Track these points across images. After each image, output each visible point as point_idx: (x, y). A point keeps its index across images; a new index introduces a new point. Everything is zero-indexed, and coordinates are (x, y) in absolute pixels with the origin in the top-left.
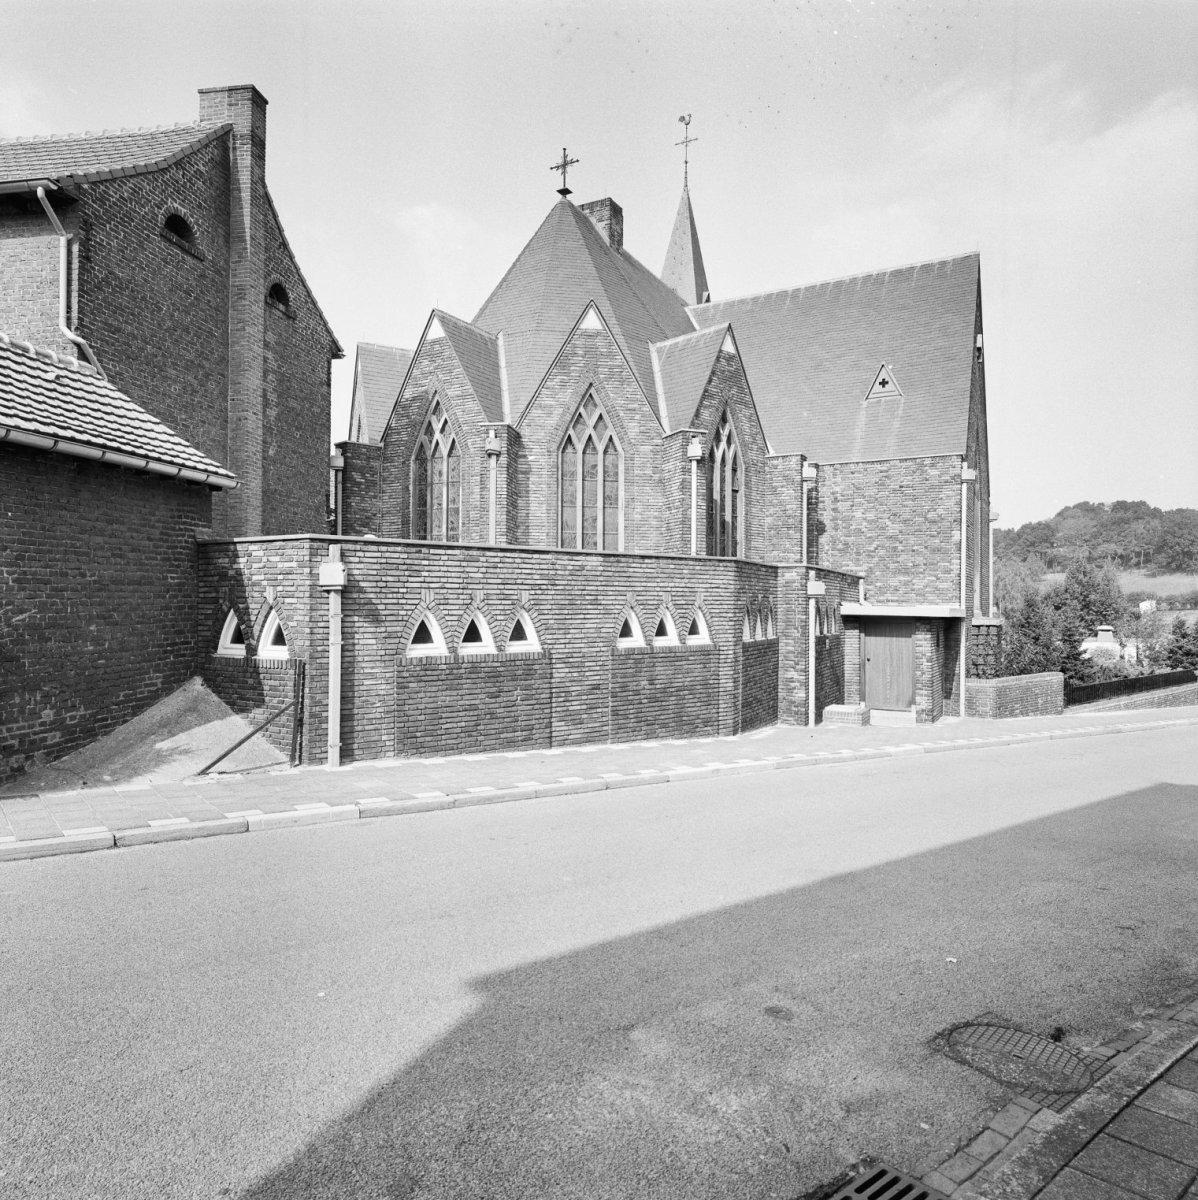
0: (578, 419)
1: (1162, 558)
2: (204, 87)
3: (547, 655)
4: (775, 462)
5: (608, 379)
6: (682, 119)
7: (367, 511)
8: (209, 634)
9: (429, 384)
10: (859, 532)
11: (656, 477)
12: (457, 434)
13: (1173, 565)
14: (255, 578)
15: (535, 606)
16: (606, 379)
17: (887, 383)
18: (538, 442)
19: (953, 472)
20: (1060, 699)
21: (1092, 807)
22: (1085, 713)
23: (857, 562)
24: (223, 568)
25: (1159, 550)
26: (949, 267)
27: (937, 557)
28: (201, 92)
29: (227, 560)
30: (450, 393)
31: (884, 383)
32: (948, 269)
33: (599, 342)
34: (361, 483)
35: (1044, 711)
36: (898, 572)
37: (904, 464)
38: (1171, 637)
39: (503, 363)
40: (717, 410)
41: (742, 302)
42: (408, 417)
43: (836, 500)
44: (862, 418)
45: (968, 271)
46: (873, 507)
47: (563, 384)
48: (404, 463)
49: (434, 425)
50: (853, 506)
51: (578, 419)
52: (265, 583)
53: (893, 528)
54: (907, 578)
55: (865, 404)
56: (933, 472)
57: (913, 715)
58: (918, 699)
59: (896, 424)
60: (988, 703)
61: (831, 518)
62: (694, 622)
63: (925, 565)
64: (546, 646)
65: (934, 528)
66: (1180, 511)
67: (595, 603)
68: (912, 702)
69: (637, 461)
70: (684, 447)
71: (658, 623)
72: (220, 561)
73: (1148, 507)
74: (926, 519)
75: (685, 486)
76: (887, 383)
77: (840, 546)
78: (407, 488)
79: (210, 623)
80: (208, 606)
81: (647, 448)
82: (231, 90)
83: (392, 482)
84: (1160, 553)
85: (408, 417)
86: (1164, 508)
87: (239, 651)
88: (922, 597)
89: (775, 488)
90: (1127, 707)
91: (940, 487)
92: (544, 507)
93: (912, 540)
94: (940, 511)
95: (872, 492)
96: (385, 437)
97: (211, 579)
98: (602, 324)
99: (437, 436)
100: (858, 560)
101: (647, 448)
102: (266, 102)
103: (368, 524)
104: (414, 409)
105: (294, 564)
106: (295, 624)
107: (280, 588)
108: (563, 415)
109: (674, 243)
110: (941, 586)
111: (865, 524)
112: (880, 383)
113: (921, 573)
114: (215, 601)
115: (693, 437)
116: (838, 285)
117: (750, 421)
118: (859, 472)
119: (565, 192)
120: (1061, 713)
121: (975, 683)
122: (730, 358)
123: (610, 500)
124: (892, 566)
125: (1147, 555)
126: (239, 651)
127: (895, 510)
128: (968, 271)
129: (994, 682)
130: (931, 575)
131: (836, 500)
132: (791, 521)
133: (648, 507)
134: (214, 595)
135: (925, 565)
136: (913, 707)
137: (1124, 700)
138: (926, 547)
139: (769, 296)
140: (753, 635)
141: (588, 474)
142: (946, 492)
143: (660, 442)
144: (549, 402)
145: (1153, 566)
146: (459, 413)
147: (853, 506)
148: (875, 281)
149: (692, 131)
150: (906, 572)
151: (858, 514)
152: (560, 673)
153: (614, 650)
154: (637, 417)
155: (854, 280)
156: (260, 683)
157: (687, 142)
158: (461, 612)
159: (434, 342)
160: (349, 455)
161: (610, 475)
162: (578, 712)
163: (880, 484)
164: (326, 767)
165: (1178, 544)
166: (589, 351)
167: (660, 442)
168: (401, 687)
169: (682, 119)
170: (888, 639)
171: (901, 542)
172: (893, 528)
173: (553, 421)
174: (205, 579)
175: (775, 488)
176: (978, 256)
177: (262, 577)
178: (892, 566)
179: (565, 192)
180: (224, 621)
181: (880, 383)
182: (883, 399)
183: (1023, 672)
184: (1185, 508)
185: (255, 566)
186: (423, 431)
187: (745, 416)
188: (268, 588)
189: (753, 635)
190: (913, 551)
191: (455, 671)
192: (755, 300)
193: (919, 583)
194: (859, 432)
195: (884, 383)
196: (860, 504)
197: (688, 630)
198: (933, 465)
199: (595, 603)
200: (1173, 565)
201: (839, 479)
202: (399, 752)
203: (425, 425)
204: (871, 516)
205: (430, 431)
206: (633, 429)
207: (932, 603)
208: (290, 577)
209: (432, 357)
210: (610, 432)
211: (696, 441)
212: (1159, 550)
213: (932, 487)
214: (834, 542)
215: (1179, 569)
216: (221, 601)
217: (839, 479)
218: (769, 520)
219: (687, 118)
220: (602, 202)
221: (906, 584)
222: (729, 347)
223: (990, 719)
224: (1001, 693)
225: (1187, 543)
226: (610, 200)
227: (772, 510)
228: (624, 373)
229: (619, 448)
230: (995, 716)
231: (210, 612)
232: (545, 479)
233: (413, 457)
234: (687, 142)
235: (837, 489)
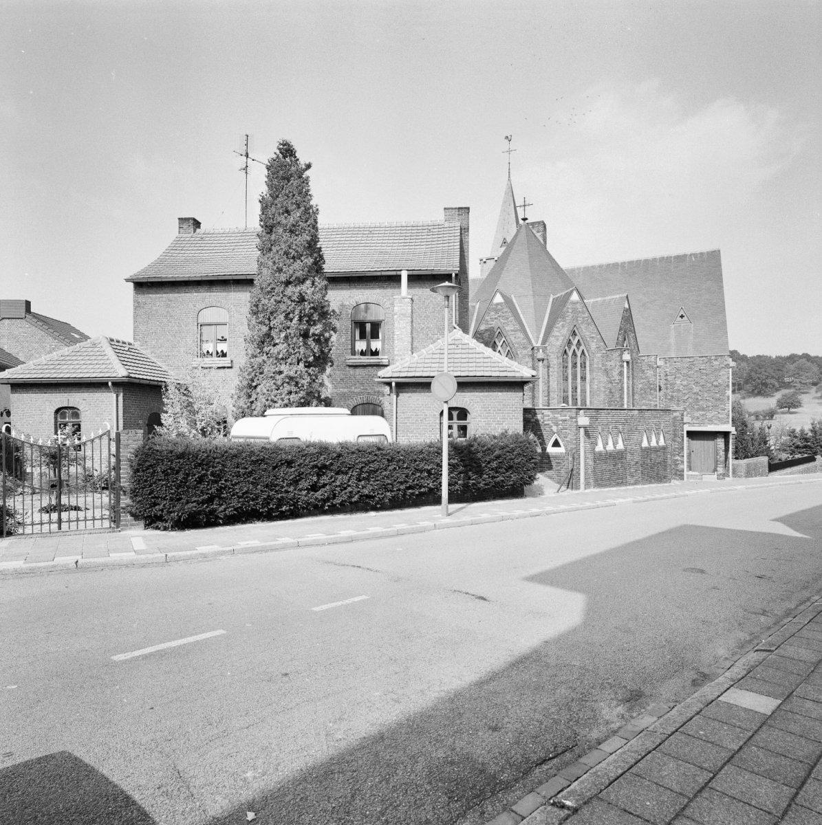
0: (570, 343)
1: (748, 387)
2: (447, 207)
4: (643, 358)
5: (582, 323)
6: (507, 137)
9: (494, 324)
10: (679, 391)
11: (603, 368)
13: (756, 391)
14: (546, 422)
16: (582, 323)
18: (553, 353)
19: (725, 363)
20: (767, 470)
21: (758, 534)
22: (777, 475)
23: (678, 405)
25: (747, 382)
26: (705, 256)
27: (718, 403)
28: (445, 209)
30: (507, 328)
31: (682, 316)
32: (705, 256)
35: (762, 475)
36: (699, 410)
37: (702, 359)
39: (520, 312)
41: (593, 267)
43: (667, 375)
44: (673, 333)
45: (715, 256)
47: (563, 326)
49: (498, 343)
51: (570, 343)
53: (696, 389)
54: (703, 413)
55: (673, 326)
57: (716, 476)
58: (718, 469)
59: (691, 338)
60: (742, 471)
65: (717, 389)
66: (759, 357)
68: (715, 470)
70: (621, 355)
73: (739, 354)
75: (621, 373)
77: (669, 397)
81: (599, 355)
82: (459, 208)
84: (747, 384)
86: (749, 355)
88: (711, 421)
89: (644, 371)
90: (791, 473)
93: (706, 395)
94: (720, 381)
101: (599, 355)
104: (487, 335)
109: (503, 211)
110: (720, 416)
111: (682, 387)
116: (646, 261)
118: (678, 362)
120: (767, 476)
121: (737, 462)
123: (583, 379)
124: (696, 407)
125: (739, 385)
128: (715, 256)
129: (746, 461)
131: (667, 375)
132: (652, 386)
133: (600, 382)
136: (716, 473)
137: (789, 470)
139: (608, 265)
140: (649, 442)
141: (575, 365)
142: (722, 372)
143: (605, 352)
144: (558, 334)
145: (743, 392)
148: (666, 260)
149: (513, 145)
150: (703, 409)
151: (678, 382)
152: (629, 457)
155: (655, 260)
156: (550, 461)
157: (509, 151)
159: (498, 304)
161: (583, 366)
163: (690, 368)
164: (581, 491)
165: (759, 379)
166: (574, 310)
167: (605, 352)
169: (507, 137)
170: (702, 442)
172: (696, 389)
173: (559, 343)
175: (644, 371)
176: (719, 251)
178: (696, 407)
182: (682, 325)
183: (752, 456)
184: (761, 355)
189: (615, 444)
192: (601, 266)
193: (709, 415)
194: (672, 340)
196: (679, 378)
200: (756, 391)
201: (668, 365)
202: (595, 487)
204: (685, 383)
206: (593, 346)
207: (716, 424)
209: (497, 311)
210: (582, 347)
211: (626, 352)
212: (747, 382)
213: (716, 370)
215: (760, 394)
217: (668, 365)
218: (640, 386)
219: (509, 137)
220: (539, 223)
221: (703, 415)
223: (744, 478)
224: (748, 465)
225: (764, 377)
226: (543, 222)
227: (642, 381)
229: (587, 355)
230: (746, 477)
232: (556, 370)
234: (509, 151)
235: (668, 370)
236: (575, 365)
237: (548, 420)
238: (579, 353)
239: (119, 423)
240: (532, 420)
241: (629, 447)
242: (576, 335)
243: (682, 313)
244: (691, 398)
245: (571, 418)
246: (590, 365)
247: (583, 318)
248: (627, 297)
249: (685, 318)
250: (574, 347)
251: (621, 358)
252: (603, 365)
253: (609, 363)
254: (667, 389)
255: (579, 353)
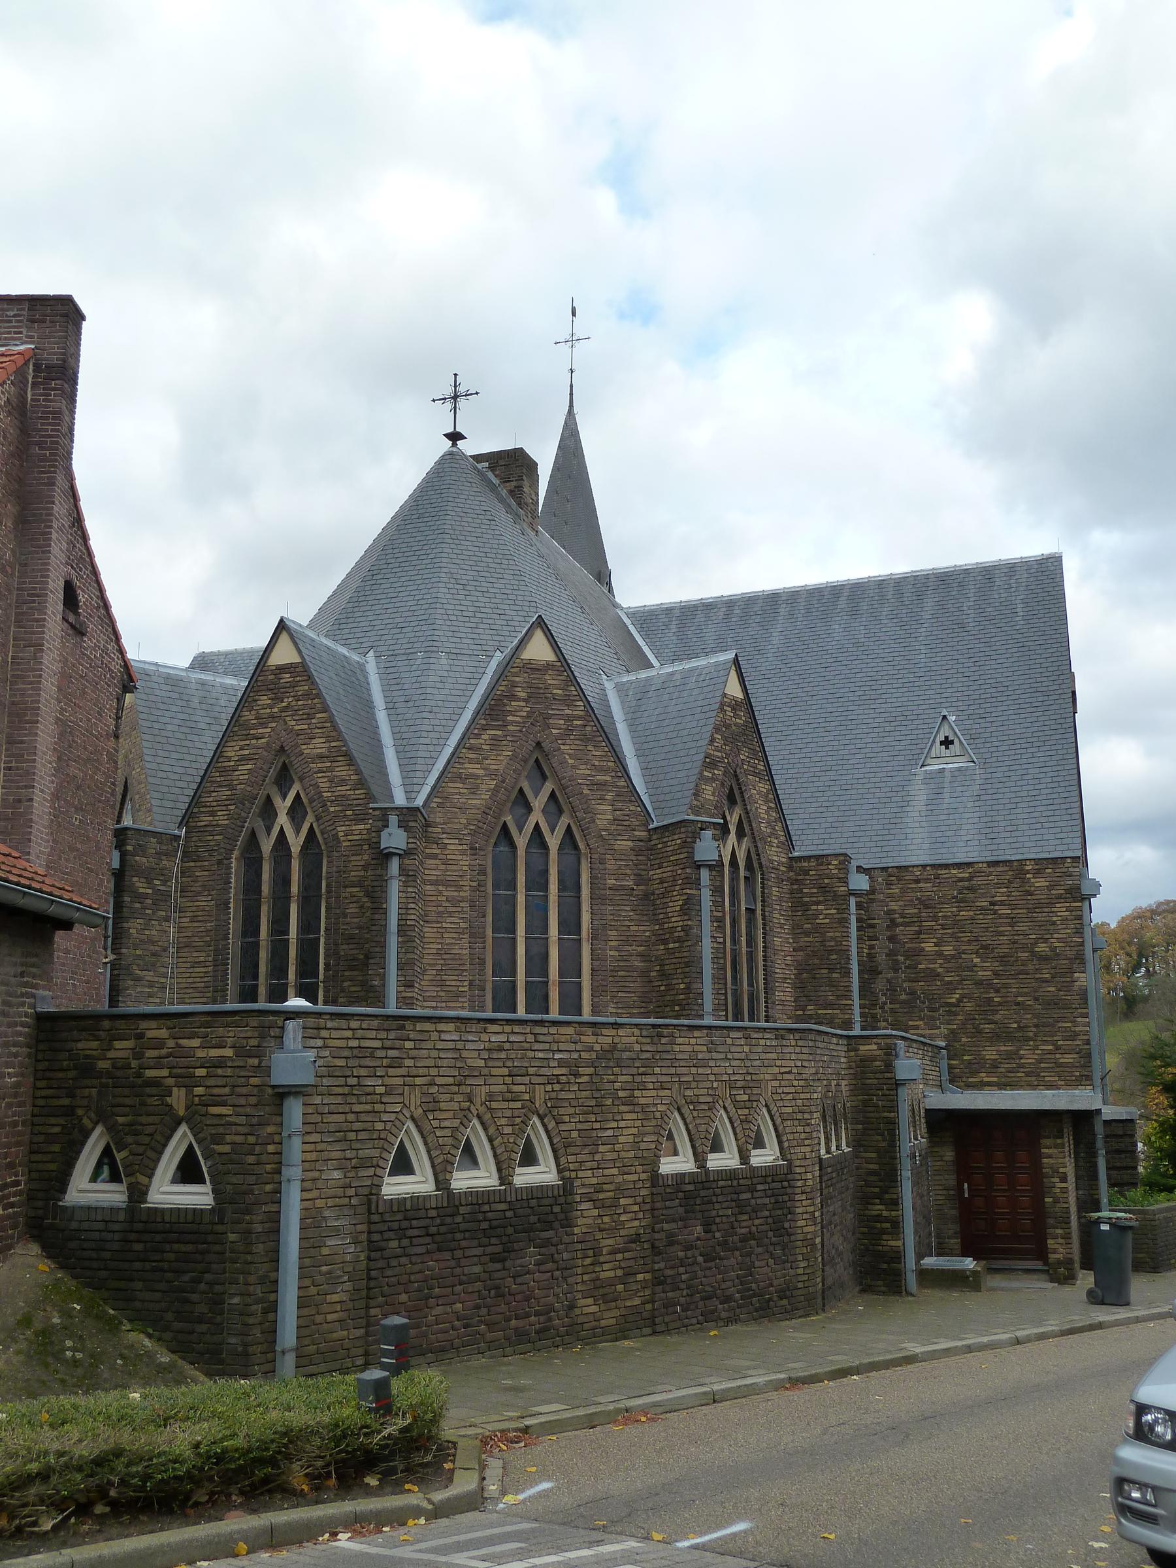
3: (567, 1186)
5: (564, 736)
7: (153, 943)
8: (53, 1167)
10: (932, 975)
12: (318, 818)
14: (150, 1073)
15: (550, 1114)
16: (564, 736)
17: (952, 742)
24: (87, 1057)
29: (95, 1044)
30: (307, 750)
31: (947, 743)
33: (551, 679)
34: (146, 896)
36: (996, 1038)
38: (311, 1055)
40: (722, 785)
42: (231, 787)
46: (952, 936)
47: (495, 741)
48: (220, 862)
49: (277, 801)
50: (919, 933)
52: (171, 1081)
56: (1041, 882)
61: (887, 950)
62: (759, 1132)
63: (1036, 1026)
64: (567, 1174)
67: (630, 1102)
69: (611, 863)
71: (753, 1135)
72: (80, 1045)
74: (1033, 954)
76: (952, 742)
78: (226, 904)
79: (56, 1148)
80: (53, 1120)
83: (199, 894)
85: (231, 787)
87: (112, 1195)
91: (1050, 905)
92: (466, 938)
95: (947, 911)
96: (187, 820)
97: (61, 1075)
98: (557, 655)
99: (283, 819)
100: (933, 1019)
102: (83, 318)
103: (153, 965)
105: (229, 1052)
106: (226, 1149)
107: (199, 1090)
108: (496, 791)
112: (942, 743)
113: (1031, 1039)
114: (69, 1111)
115: (702, 829)
117: (767, 801)
118: (927, 881)
119: (455, 437)
122: (735, 705)
126: (112, 1195)
127: (985, 940)
130: (1045, 1043)
131: (893, 924)
134: (66, 1101)
135: (1036, 1026)
138: (1036, 999)
146: (323, 784)
147: (919, 933)
151: (929, 946)
152: (586, 1216)
153: (655, 1177)
154: (609, 796)
158: (456, 1123)
159: (282, 669)
160: (129, 848)
162: (611, 1283)
168: (372, 1246)
171: (997, 991)
172: (985, 969)
173: (480, 800)
174: (48, 1074)
177: (165, 1072)
179: (455, 437)
180: (83, 1144)
181: (942, 743)
185: (150, 1053)
186: (255, 809)
187: (759, 793)
188: (175, 1090)
190: (1018, 1004)
191: (448, 1220)
195: (947, 743)
196: (930, 932)
197: (752, 1141)
198: (1038, 873)
199: (630, 1102)
203: (260, 801)
205: (268, 811)
207: (1051, 1086)
208: (220, 1071)
213: (1039, 905)
214: (893, 989)
216: (80, 1112)
221: (1010, 1056)
222: (734, 689)
228: (589, 728)
231: (56, 1130)
233: (236, 854)
236: (538, 882)
237: (159, 1066)
238: (553, 842)
239: (339, 1041)
240: (103, 1065)
241: (587, 1177)
242: (544, 777)
243: (945, 732)
244: (970, 997)
245: (242, 1052)
246: (593, 879)
247: (568, 719)
248: (736, 661)
249: (955, 748)
250: (536, 817)
251: (692, 854)
252: (640, 879)
253: (655, 874)
254: (896, 971)
255: (553, 842)
